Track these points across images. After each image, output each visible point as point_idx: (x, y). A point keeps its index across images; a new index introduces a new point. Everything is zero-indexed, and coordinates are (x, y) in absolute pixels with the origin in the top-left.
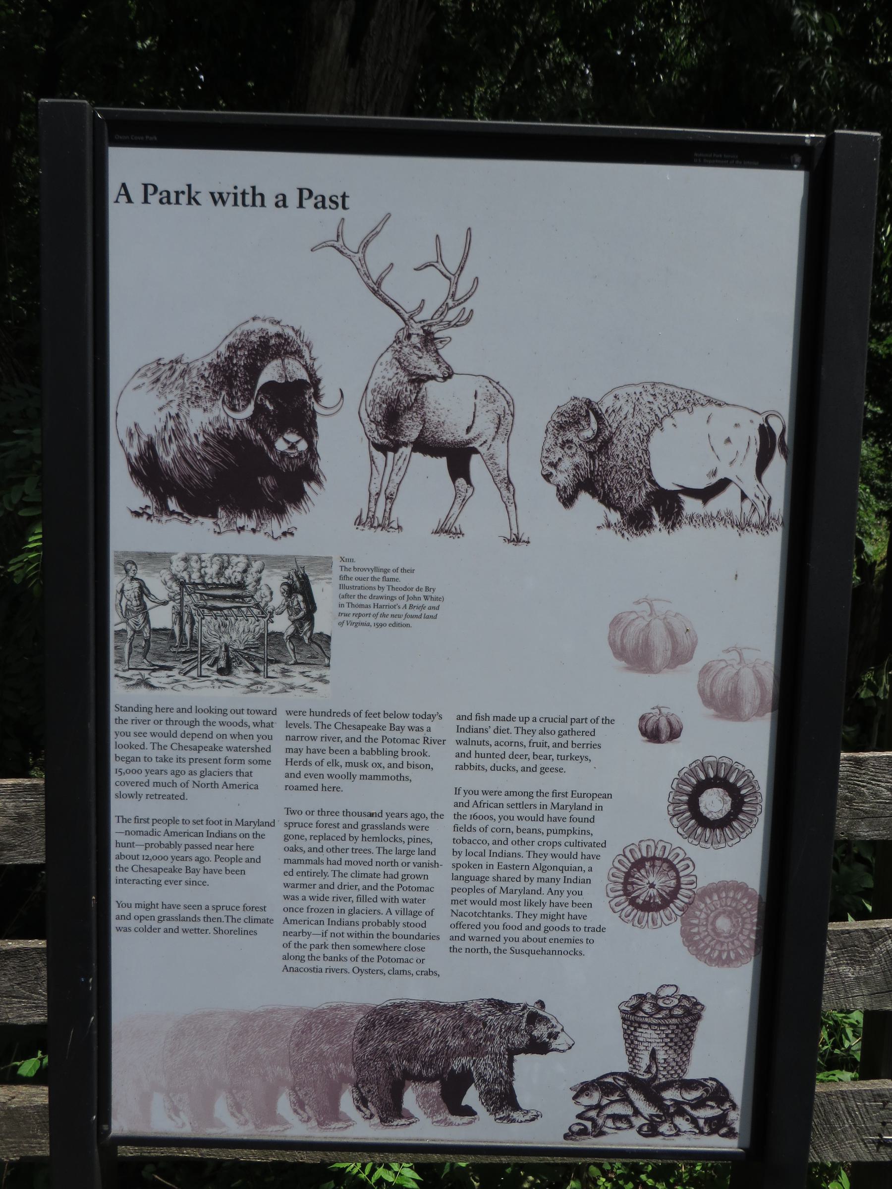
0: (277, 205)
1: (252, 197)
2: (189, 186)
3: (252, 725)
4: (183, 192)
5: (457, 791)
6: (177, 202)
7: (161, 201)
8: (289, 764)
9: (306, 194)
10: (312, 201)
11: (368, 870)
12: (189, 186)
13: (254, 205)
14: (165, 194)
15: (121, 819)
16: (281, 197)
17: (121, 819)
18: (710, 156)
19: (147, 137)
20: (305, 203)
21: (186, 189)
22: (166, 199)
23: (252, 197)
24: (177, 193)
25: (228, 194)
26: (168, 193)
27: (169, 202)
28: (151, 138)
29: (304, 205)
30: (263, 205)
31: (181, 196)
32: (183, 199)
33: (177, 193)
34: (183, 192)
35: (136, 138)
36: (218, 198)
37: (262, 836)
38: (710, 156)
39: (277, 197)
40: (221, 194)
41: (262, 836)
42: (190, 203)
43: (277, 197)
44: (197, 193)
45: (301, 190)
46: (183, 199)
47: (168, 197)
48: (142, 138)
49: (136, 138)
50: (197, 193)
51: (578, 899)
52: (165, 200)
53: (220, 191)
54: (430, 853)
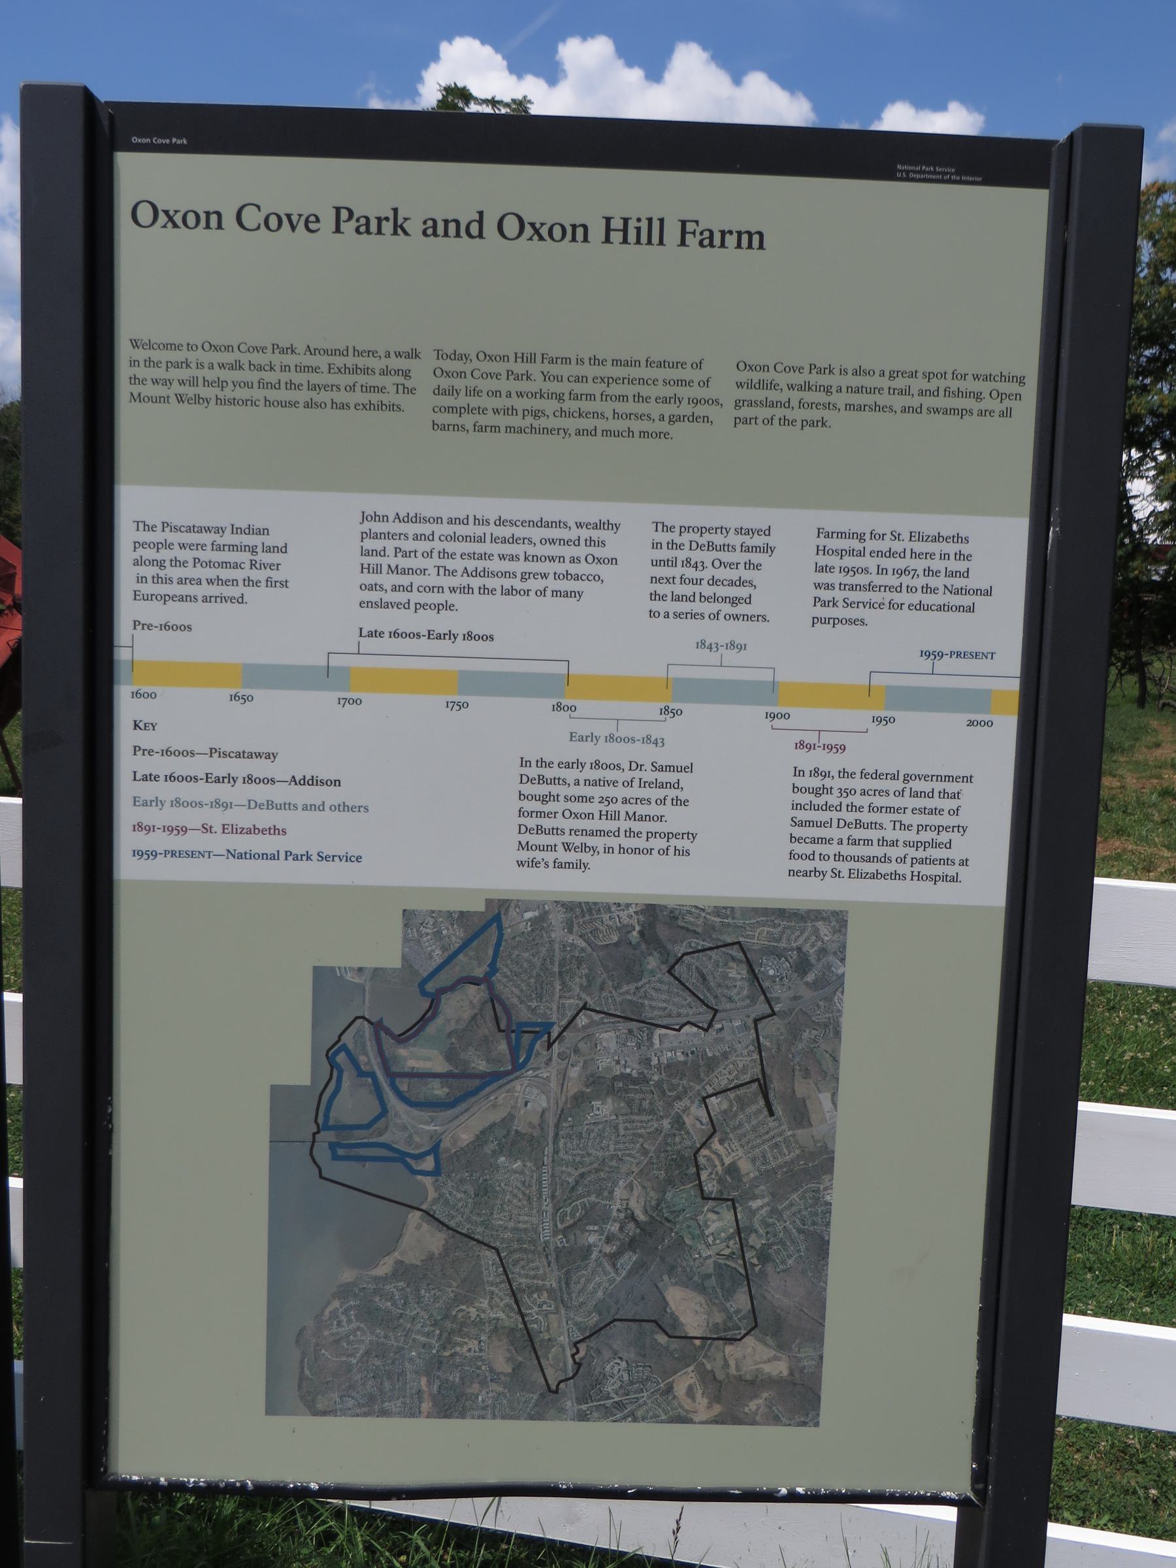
0: (425, 233)
1: (651, 232)
2: (395, 210)
3: (574, 527)
4: (387, 219)
5: (364, 517)
6: (379, 232)
7: (357, 231)
8: (821, 553)
9: (344, 214)
10: (353, 224)
11: (479, 548)
12: (395, 210)
13: (446, 234)
14: (363, 221)
15: (141, 526)
16: (430, 223)
17: (141, 526)
18: (918, 168)
19: (174, 140)
20: (343, 226)
21: (391, 215)
22: (365, 227)
23: (651, 232)
24: (379, 220)
25: (300, 216)
26: (367, 219)
27: (368, 232)
28: (179, 142)
29: (342, 230)
30: (220, 227)
31: (384, 222)
32: (388, 227)
33: (379, 220)
34: (387, 219)
35: (160, 141)
36: (431, 229)
37: (757, 567)
38: (918, 168)
39: (425, 223)
40: (289, 216)
41: (757, 567)
42: (395, 233)
43: (425, 223)
44: (406, 219)
45: (338, 210)
46: (388, 227)
47: (368, 224)
48: (168, 141)
49: (160, 141)
50: (406, 219)
51: (598, 552)
52: (363, 229)
53: (288, 212)
54: (961, 575)
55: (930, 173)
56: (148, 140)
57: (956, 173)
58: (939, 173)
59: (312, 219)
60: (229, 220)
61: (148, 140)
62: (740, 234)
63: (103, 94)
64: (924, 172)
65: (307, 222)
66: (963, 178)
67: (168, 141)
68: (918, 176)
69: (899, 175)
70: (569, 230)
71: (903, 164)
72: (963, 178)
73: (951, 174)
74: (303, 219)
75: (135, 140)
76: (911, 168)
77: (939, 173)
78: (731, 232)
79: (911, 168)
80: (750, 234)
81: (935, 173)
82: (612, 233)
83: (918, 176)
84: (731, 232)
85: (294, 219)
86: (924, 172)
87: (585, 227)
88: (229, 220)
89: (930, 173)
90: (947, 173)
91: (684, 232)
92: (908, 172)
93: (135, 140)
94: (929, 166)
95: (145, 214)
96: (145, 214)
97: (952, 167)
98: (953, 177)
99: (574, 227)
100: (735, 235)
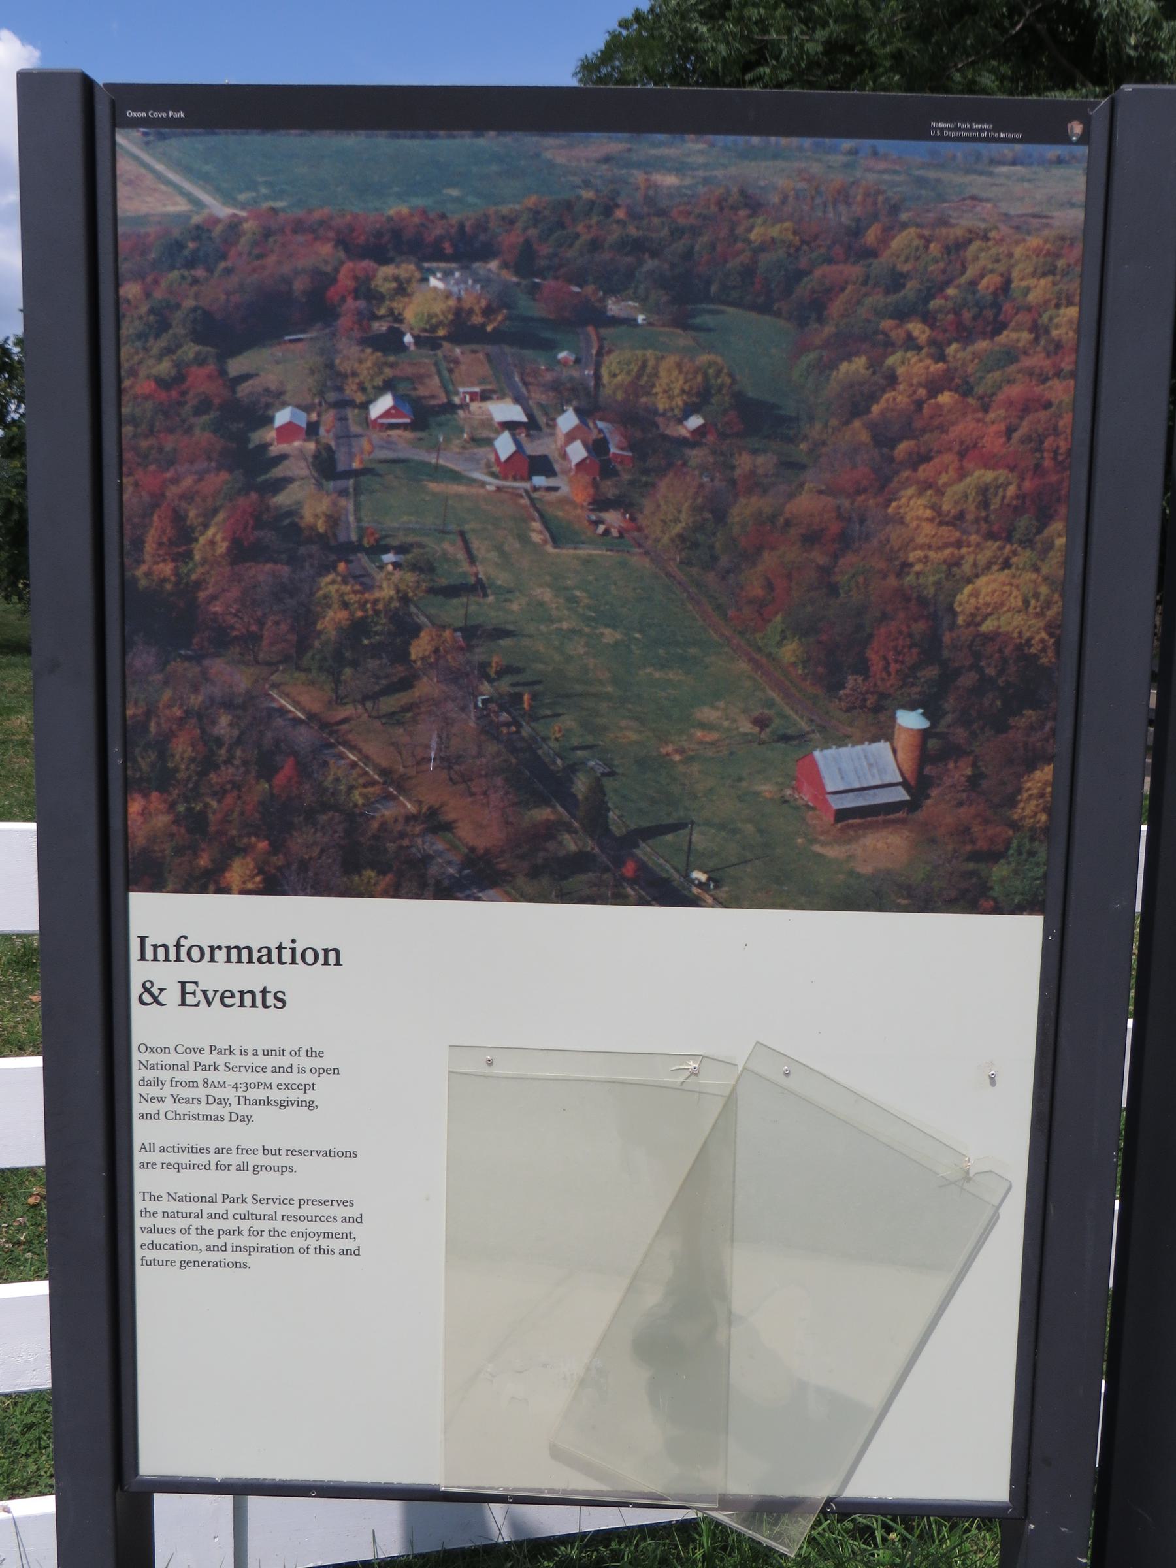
18: (953, 126)
19: (171, 113)
28: (176, 115)
31: (217, 951)
35: (156, 115)
38: (953, 126)
48: (164, 115)
55: (966, 130)
56: (143, 114)
57: (994, 130)
58: (975, 130)
59: (228, 994)
60: (172, 1050)
61: (143, 114)
62: (229, 949)
63: (101, 77)
64: (960, 130)
65: (222, 998)
66: (1002, 135)
67: (164, 115)
68: (953, 134)
69: (933, 133)
70: (207, 952)
71: (937, 121)
72: (1002, 135)
73: (989, 131)
74: (218, 995)
75: (130, 114)
76: (945, 125)
77: (975, 130)
78: (219, 948)
79: (945, 125)
80: (239, 949)
81: (971, 130)
82: (227, 1501)
83: (953, 134)
84: (219, 948)
85: (210, 994)
86: (960, 130)
87: (337, 951)
88: (172, 1050)
89: (966, 130)
90: (984, 130)
91: (184, 993)
92: (942, 130)
93: (130, 114)
94: (952, 122)
95: (143, 1048)
96: (143, 1048)
97: (989, 123)
98: (992, 134)
99: (326, 951)
100: (225, 950)
